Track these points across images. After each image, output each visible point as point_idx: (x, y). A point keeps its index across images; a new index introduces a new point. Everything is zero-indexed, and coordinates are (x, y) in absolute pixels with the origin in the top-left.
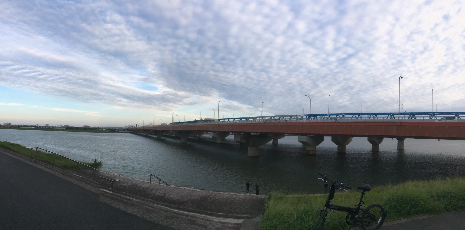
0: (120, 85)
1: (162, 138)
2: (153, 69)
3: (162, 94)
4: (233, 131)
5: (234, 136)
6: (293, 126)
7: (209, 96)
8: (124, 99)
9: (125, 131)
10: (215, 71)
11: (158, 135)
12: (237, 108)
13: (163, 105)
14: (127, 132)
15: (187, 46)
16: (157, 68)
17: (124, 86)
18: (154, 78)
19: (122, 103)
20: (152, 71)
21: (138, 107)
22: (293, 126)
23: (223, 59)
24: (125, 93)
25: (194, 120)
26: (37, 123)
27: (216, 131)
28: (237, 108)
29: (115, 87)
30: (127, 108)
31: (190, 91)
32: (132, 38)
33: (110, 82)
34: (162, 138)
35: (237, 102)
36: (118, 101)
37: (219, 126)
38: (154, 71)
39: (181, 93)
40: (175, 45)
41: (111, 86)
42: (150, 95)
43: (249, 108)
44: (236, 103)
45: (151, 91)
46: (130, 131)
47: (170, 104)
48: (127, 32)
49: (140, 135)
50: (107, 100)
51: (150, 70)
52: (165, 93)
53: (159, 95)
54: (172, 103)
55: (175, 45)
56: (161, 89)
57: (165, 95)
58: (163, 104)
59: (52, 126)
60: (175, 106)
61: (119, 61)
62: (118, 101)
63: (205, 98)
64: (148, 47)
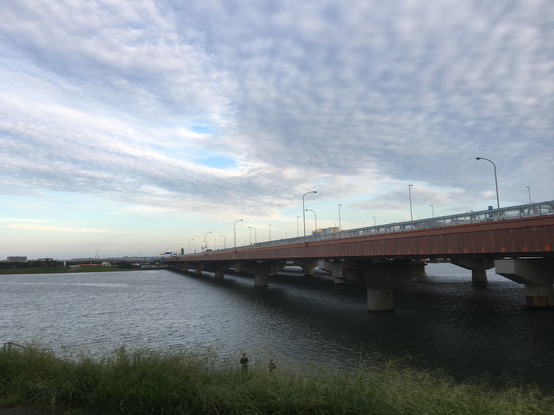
0: (149, 153)
1: (227, 277)
2: (223, 115)
3: (247, 176)
4: (435, 252)
5: (471, 272)
6: (427, 238)
7: (355, 173)
8: (160, 189)
9: (154, 264)
10: (367, 111)
11: (217, 272)
12: (425, 198)
13: (250, 202)
14: (160, 267)
15: (298, 52)
16: (233, 113)
17: (158, 156)
18: (228, 138)
19: (156, 198)
20: (222, 122)
21: (195, 209)
22: (427, 238)
23: (386, 76)
24: (162, 174)
25: (280, 239)
26: (182, 248)
27: (331, 258)
28: (425, 198)
29: (136, 158)
30: (168, 209)
31: (310, 164)
32: (174, 36)
33: (125, 148)
34: (227, 277)
35: (424, 183)
36: (145, 193)
37: (307, 246)
38: (225, 121)
39: (291, 173)
40: (273, 52)
41: (125, 155)
42: (219, 179)
43: (453, 196)
44: (420, 186)
45: (222, 169)
46: (166, 266)
47: (267, 199)
48: (159, 20)
49: (186, 274)
50: (119, 191)
51: (215, 117)
52: (253, 174)
53: (240, 179)
54: (269, 197)
55: (273, 52)
56: (244, 163)
57: (255, 177)
58: (250, 200)
59: (106, 257)
60: (276, 202)
61: (143, 92)
62: (145, 193)
63: (344, 180)
64: (209, 59)
